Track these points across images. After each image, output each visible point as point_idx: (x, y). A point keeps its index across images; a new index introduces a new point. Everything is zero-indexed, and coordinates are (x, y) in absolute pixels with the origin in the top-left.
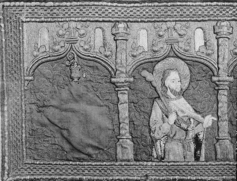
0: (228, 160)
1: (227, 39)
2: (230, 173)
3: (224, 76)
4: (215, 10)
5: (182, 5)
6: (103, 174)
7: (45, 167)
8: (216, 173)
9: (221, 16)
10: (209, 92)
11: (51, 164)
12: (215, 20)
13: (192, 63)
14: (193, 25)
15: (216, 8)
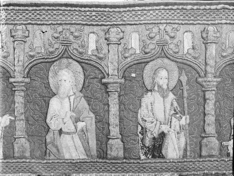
0: (26, 158)
1: (23, 42)
2: (27, 171)
3: (18, 78)
4: (12, 14)
5: (17, 9)
6: (33, 171)
7: (118, 165)
8: (13, 170)
9: (18, 20)
10: (7, 93)
11: (26, 162)
12: (12, 24)
13: (184, 65)
14: (87, 29)
15: (13, 12)
